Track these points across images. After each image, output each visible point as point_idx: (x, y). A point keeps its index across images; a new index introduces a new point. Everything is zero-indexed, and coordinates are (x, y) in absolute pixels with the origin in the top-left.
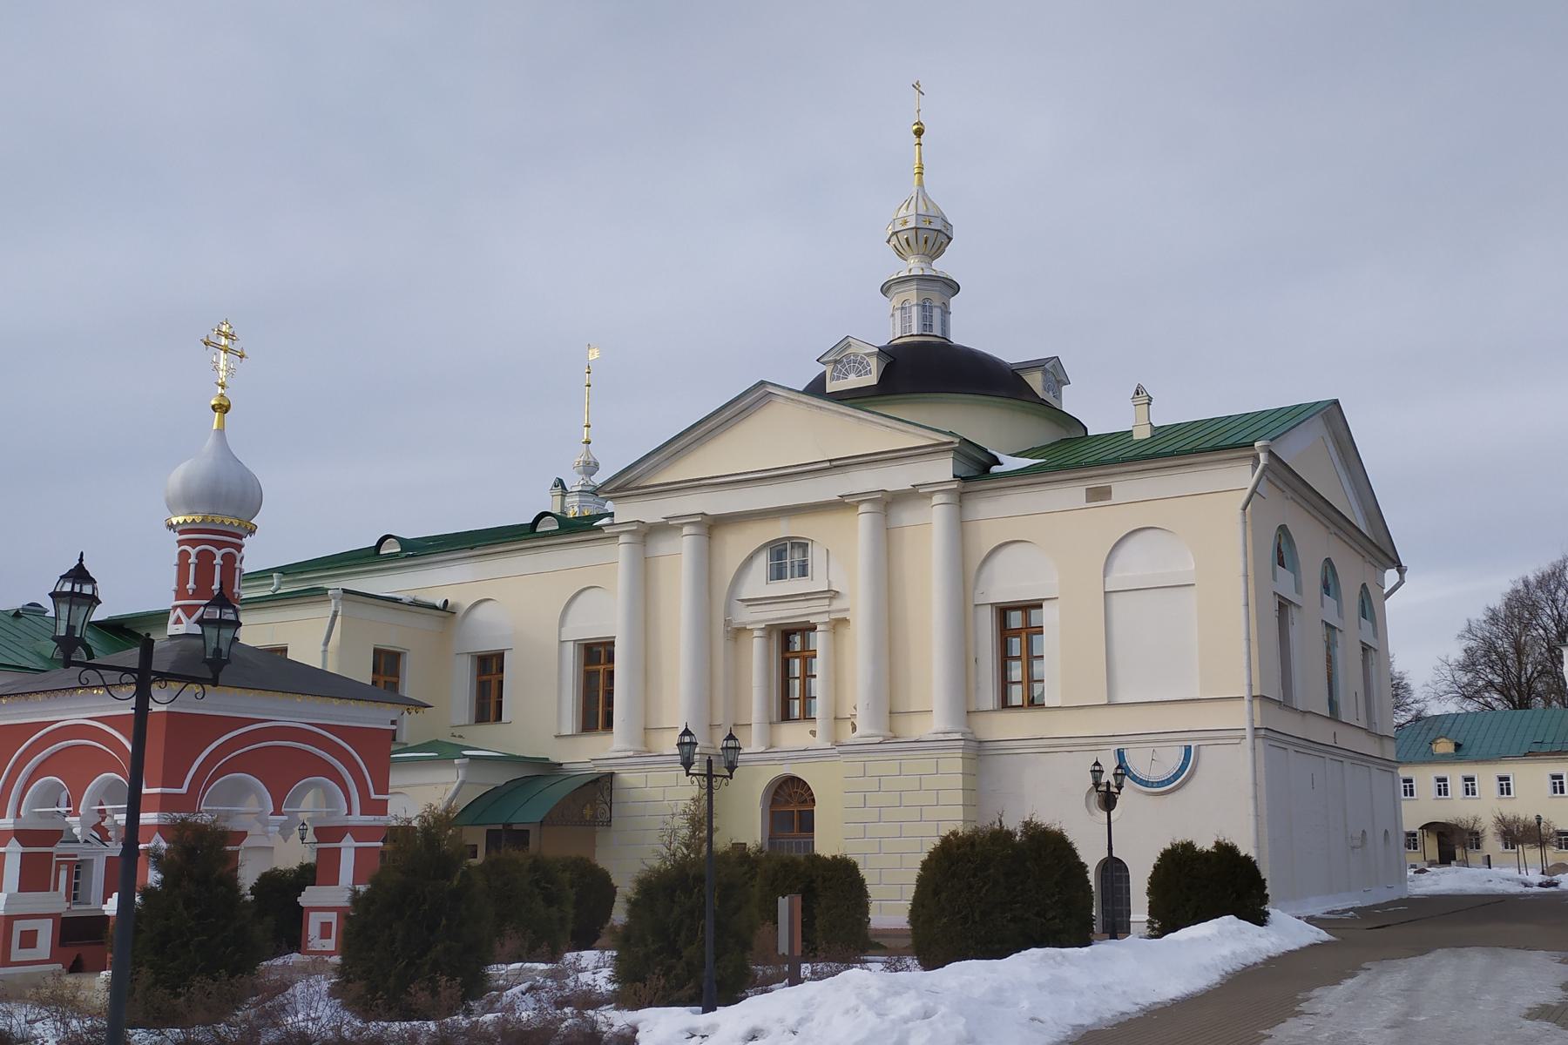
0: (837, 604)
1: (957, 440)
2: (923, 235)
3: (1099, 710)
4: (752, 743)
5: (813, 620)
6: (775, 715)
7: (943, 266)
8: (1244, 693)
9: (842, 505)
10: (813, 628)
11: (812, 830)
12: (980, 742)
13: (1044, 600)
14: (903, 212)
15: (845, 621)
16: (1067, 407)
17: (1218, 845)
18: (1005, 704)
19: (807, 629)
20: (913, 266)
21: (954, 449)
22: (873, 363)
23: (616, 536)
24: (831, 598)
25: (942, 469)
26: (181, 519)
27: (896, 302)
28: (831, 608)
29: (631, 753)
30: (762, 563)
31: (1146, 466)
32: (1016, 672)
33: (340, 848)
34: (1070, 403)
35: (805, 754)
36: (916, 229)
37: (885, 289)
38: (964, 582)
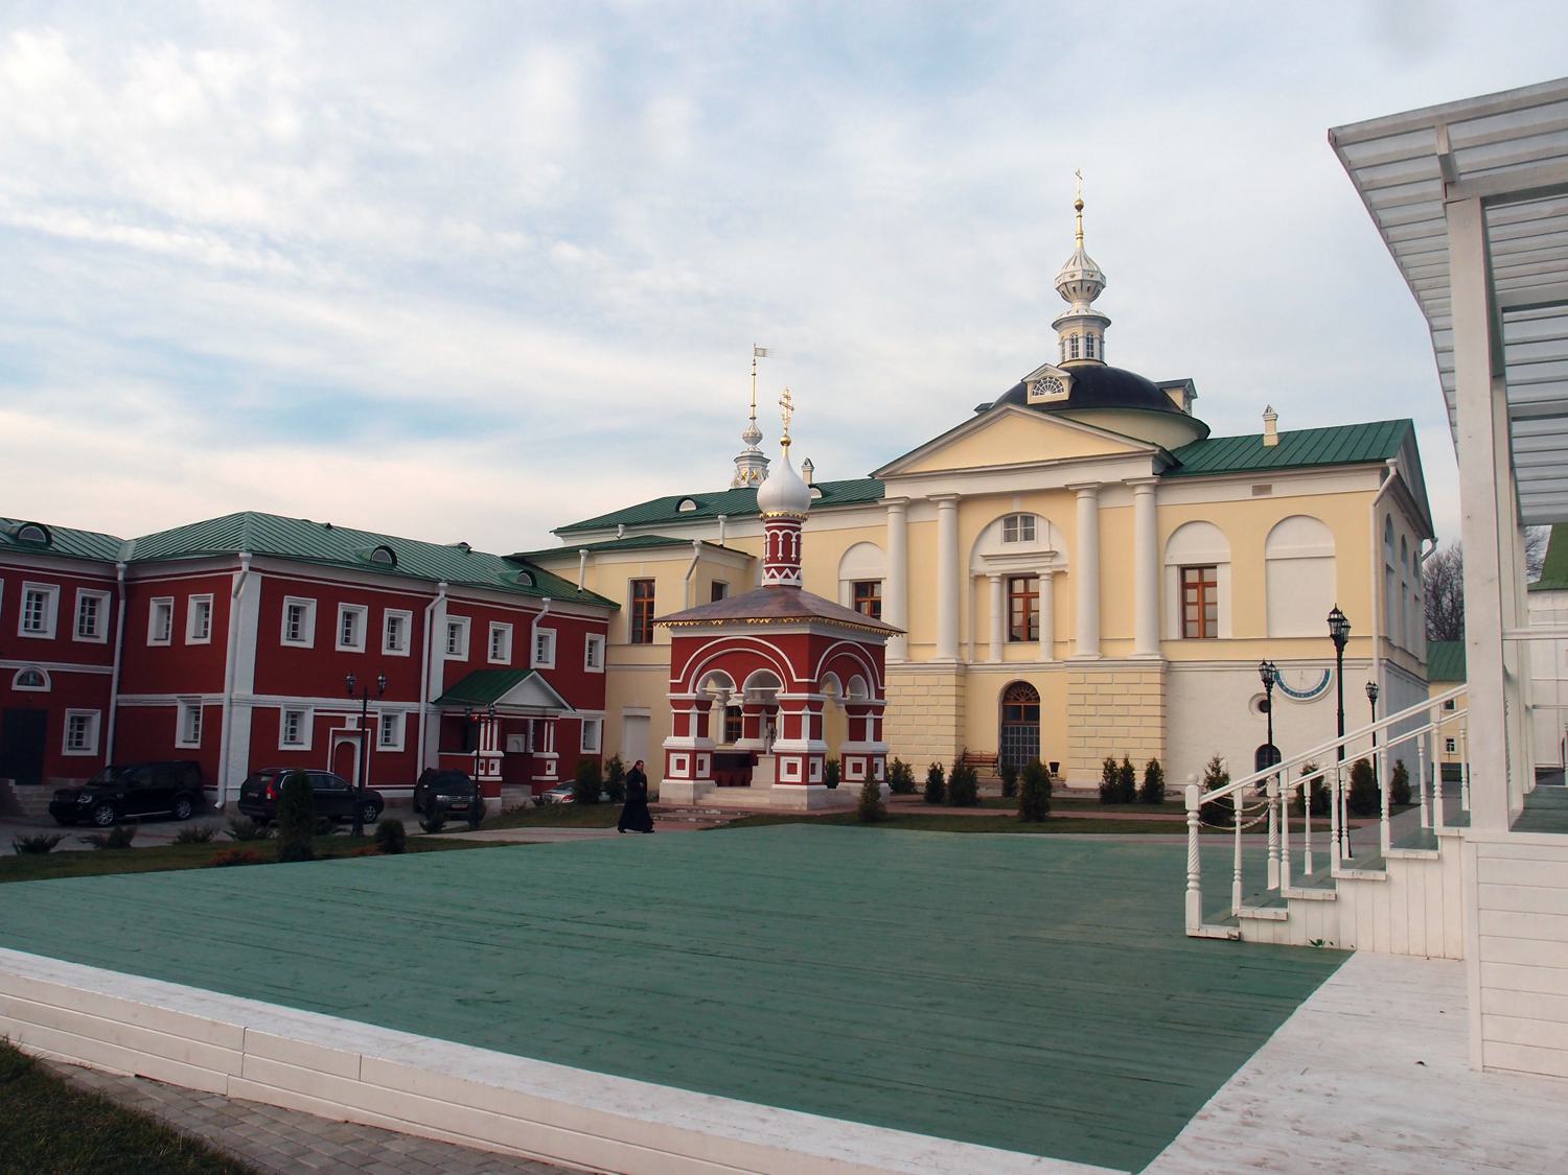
0: (1056, 562)
1: (1158, 449)
3: (1322, 642)
5: (1038, 572)
6: (1006, 638)
7: (1099, 307)
8: (1373, 633)
9: (1067, 492)
10: (1036, 577)
11: (1038, 719)
14: (1071, 268)
16: (1195, 415)
19: (1028, 577)
20: (1077, 308)
22: (1066, 386)
23: (886, 507)
25: (1145, 469)
27: (1067, 334)
29: (902, 662)
30: (998, 530)
31: (1312, 471)
32: (1019, 604)
33: (865, 719)
34: (1198, 411)
35: (1034, 666)
36: (1082, 281)
37: (1056, 325)
38: (1158, 549)
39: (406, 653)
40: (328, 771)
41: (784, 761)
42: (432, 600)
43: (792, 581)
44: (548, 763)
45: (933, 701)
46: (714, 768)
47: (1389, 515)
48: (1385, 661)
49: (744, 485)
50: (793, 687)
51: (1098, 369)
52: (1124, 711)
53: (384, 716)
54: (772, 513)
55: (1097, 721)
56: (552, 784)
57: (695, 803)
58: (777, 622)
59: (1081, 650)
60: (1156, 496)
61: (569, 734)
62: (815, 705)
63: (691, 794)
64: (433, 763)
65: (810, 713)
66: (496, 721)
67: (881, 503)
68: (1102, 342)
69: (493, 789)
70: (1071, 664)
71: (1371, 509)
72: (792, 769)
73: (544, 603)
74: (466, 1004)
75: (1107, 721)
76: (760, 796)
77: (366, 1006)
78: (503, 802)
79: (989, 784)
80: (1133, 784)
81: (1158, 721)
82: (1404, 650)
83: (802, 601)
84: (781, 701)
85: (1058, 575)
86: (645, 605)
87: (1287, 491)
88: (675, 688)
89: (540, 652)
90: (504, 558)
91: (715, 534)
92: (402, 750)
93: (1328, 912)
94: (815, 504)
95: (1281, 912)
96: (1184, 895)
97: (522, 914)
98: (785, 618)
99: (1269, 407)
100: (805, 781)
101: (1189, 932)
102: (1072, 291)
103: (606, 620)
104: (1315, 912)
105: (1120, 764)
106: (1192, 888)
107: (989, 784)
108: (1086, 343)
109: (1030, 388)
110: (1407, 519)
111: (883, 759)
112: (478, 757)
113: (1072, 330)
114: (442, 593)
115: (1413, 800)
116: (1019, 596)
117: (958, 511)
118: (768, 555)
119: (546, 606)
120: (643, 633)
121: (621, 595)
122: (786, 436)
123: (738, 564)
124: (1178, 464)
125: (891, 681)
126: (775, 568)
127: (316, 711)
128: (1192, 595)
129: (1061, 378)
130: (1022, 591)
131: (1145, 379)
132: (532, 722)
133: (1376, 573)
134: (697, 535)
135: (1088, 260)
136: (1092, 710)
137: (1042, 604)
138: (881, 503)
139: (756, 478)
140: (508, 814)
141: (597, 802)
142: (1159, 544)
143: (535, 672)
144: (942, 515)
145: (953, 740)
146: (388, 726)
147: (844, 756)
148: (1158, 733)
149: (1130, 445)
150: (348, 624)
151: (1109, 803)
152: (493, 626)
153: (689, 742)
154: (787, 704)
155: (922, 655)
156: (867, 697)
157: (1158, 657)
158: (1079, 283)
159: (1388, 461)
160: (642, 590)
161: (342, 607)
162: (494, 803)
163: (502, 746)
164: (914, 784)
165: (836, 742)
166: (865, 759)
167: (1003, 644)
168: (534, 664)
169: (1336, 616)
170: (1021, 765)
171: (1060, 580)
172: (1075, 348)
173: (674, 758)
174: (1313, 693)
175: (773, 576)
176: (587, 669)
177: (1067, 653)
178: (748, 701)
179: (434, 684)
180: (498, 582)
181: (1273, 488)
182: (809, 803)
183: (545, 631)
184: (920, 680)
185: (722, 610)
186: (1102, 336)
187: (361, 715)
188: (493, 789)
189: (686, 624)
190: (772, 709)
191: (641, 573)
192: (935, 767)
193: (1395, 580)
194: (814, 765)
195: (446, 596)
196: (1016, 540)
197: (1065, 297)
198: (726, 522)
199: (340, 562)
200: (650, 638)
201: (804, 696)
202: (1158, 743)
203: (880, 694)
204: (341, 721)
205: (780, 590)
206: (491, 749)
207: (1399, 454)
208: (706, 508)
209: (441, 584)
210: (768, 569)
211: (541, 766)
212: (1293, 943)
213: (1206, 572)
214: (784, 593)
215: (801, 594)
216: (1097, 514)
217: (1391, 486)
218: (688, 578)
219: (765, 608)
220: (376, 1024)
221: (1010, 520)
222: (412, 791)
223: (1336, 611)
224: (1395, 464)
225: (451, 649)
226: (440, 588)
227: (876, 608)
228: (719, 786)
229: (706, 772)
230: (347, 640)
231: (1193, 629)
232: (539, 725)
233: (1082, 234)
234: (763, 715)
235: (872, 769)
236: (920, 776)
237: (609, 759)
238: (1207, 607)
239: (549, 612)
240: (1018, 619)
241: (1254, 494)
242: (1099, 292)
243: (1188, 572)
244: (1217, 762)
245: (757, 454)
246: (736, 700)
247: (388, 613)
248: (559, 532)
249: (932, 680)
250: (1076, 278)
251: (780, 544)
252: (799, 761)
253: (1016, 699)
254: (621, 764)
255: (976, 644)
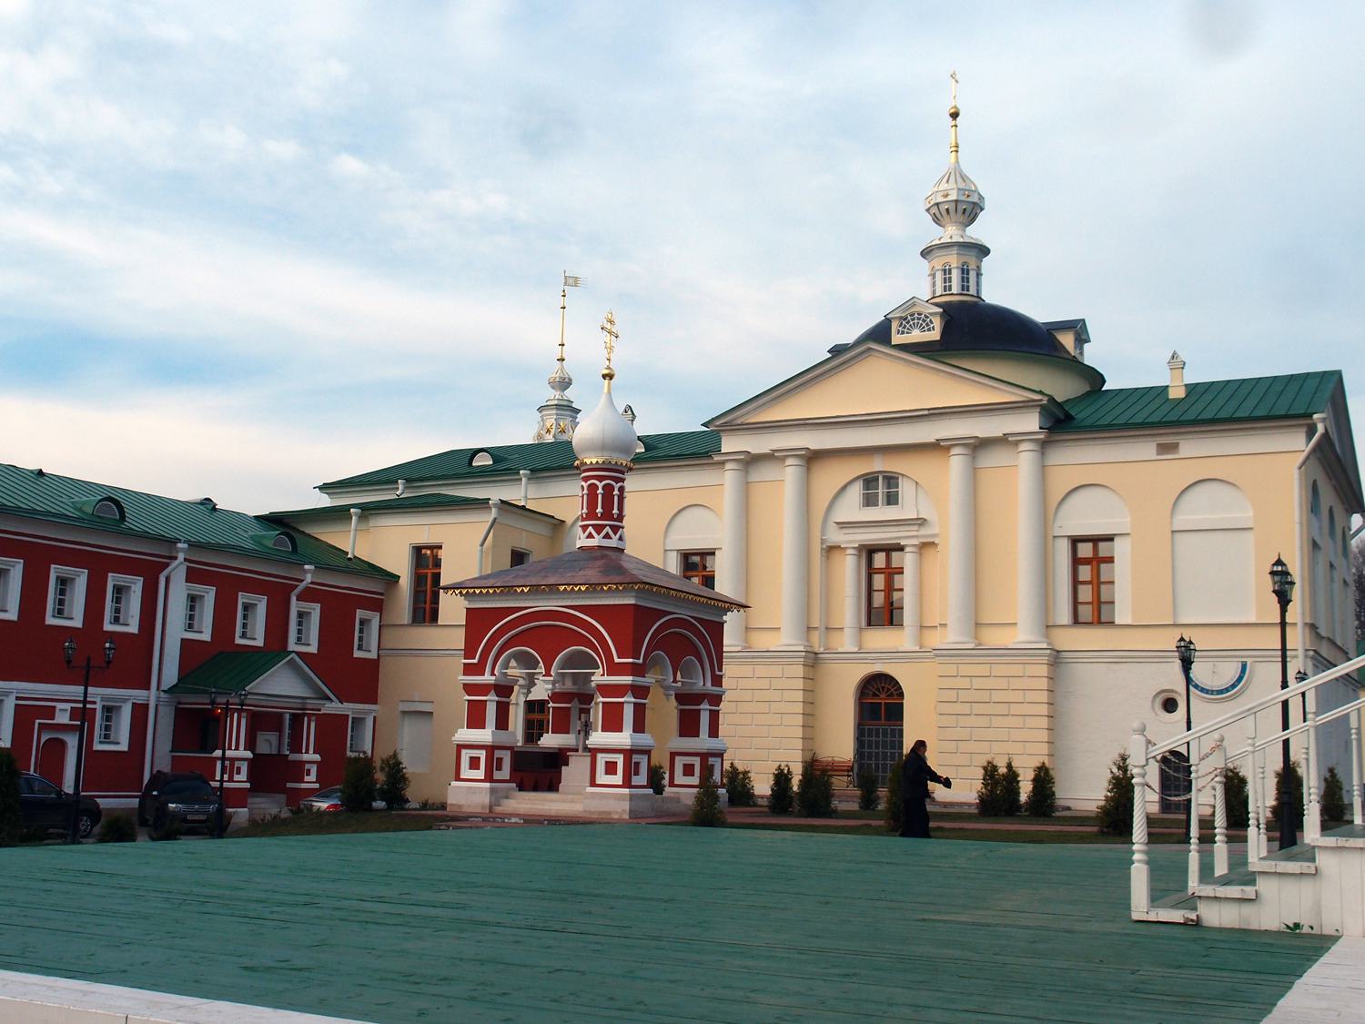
0: (923, 531)
1: (1046, 398)
2: (961, 207)
4: (846, 642)
6: (864, 623)
7: (976, 232)
9: (938, 448)
10: (901, 548)
12: (1058, 651)
13: (1115, 535)
14: (944, 186)
15: (933, 544)
17: (746, 773)
18: (1076, 621)
19: (892, 549)
20: (951, 233)
21: (1041, 406)
22: (937, 323)
23: (723, 463)
24: (920, 525)
25: (1030, 423)
26: (594, 461)
28: (919, 533)
29: (739, 649)
30: (856, 491)
32: (879, 581)
33: (699, 710)
34: (1092, 356)
36: (956, 201)
37: (925, 253)
39: (133, 628)
40: (32, 772)
41: (602, 759)
42: (167, 565)
43: (613, 542)
44: (307, 766)
45: (776, 696)
46: (514, 769)
47: (1315, 482)
48: (1312, 653)
49: (549, 439)
50: (613, 669)
51: (974, 305)
52: (1002, 709)
53: (104, 706)
54: (591, 459)
55: (972, 721)
56: (311, 792)
57: (491, 811)
58: (595, 589)
59: (952, 636)
60: (1043, 454)
61: (332, 732)
62: (641, 691)
63: (486, 800)
64: (164, 765)
65: (633, 700)
66: (244, 714)
67: (717, 458)
68: (979, 275)
69: (239, 798)
70: (939, 653)
71: (1296, 473)
72: (611, 768)
73: (306, 572)
74: (257, 971)
75: (983, 721)
76: (572, 802)
77: (125, 971)
78: (251, 813)
79: (845, 794)
80: (1018, 794)
81: (1044, 722)
82: (1332, 642)
83: (626, 565)
84: (598, 685)
85: (926, 546)
86: (429, 575)
87: (1198, 450)
88: (469, 669)
89: (299, 632)
90: (257, 518)
91: (518, 492)
92: (126, 749)
93: (1307, 887)
94: (638, 459)
95: (1249, 891)
96: (1130, 869)
97: (306, 895)
98: (606, 584)
99: (1175, 353)
100: (627, 783)
101: (1135, 916)
102: (944, 213)
103: (381, 594)
104: (1291, 889)
105: (1003, 770)
106: (1139, 861)
107: (845, 794)
108: (960, 275)
109: (894, 326)
110: (1335, 488)
111: (719, 760)
112: (223, 758)
113: (946, 259)
114: (181, 556)
115: (1347, 818)
116: (879, 571)
117: (808, 469)
118: (585, 510)
119: (309, 575)
120: (426, 612)
121: (398, 562)
122: (608, 368)
123: (542, 529)
124: (1069, 418)
125: (729, 670)
126: (592, 525)
127: (17, 698)
128: (1085, 572)
129: (931, 314)
130: (884, 566)
131: (1028, 318)
132: (287, 717)
133: (1301, 547)
134: (495, 493)
135: (964, 178)
136: (966, 708)
137: (907, 581)
138: (717, 458)
139: (563, 431)
140: (258, 824)
141: (370, 809)
142: (1046, 512)
143: (293, 655)
144: (790, 474)
145: (799, 744)
146: (108, 719)
147: (673, 755)
148: (1044, 736)
149: (1013, 393)
150: (62, 592)
151: (990, 816)
152: (243, 598)
153: (485, 735)
154: (605, 690)
155: (763, 642)
156: (702, 684)
157: (1045, 646)
158: (954, 204)
159: (1315, 416)
160: (426, 560)
161: (55, 571)
162: (240, 814)
163: (250, 745)
164: (753, 795)
165: (664, 737)
166: (698, 759)
167: (861, 629)
168: (292, 646)
169: (1280, 568)
170: (881, 774)
171: (929, 553)
172: (947, 280)
173: (466, 755)
174: (1227, 690)
175: (590, 536)
176: (357, 654)
177: (935, 640)
178: (559, 688)
179: (168, 669)
180: (249, 545)
181: (1181, 446)
182: (630, 811)
183: (306, 606)
184: (761, 670)
185: (523, 577)
186: (979, 268)
187: (81, 705)
188: (239, 798)
189: (484, 591)
190: (587, 698)
191: (424, 537)
192: (782, 771)
193: (1322, 559)
194: (637, 764)
195: (185, 560)
196: (878, 505)
197: (937, 220)
198: (529, 479)
199: (54, 515)
200: (434, 617)
201: (627, 679)
202: (1044, 749)
203: (717, 681)
204: (51, 712)
205: (598, 553)
206: (237, 748)
207: (1326, 410)
208: (505, 463)
209: (179, 545)
210: (584, 528)
211: (298, 770)
212: (1263, 929)
213: (1102, 545)
214: (603, 557)
215: (623, 557)
216: (974, 475)
217: (1318, 445)
218: (482, 545)
219: (582, 573)
220: (141, 988)
221: (869, 481)
222: (138, 800)
223: (1279, 562)
224: (1323, 420)
225: (190, 626)
226: (177, 550)
227: (709, 581)
228: (520, 790)
229: (505, 773)
230: (60, 612)
231: (1086, 612)
232: (297, 720)
233: (957, 147)
234: (574, 706)
235: (707, 771)
236: (762, 786)
237: (385, 756)
238: (1102, 587)
239: (312, 583)
240: (879, 599)
241: (1158, 454)
242: (976, 216)
243: (1081, 546)
244: (1124, 758)
245: (565, 403)
246: (541, 691)
247: (112, 579)
248: (325, 488)
249: (775, 670)
250: (949, 198)
251: (600, 497)
252: (620, 759)
253: (875, 695)
254: (401, 763)
255: (827, 628)
